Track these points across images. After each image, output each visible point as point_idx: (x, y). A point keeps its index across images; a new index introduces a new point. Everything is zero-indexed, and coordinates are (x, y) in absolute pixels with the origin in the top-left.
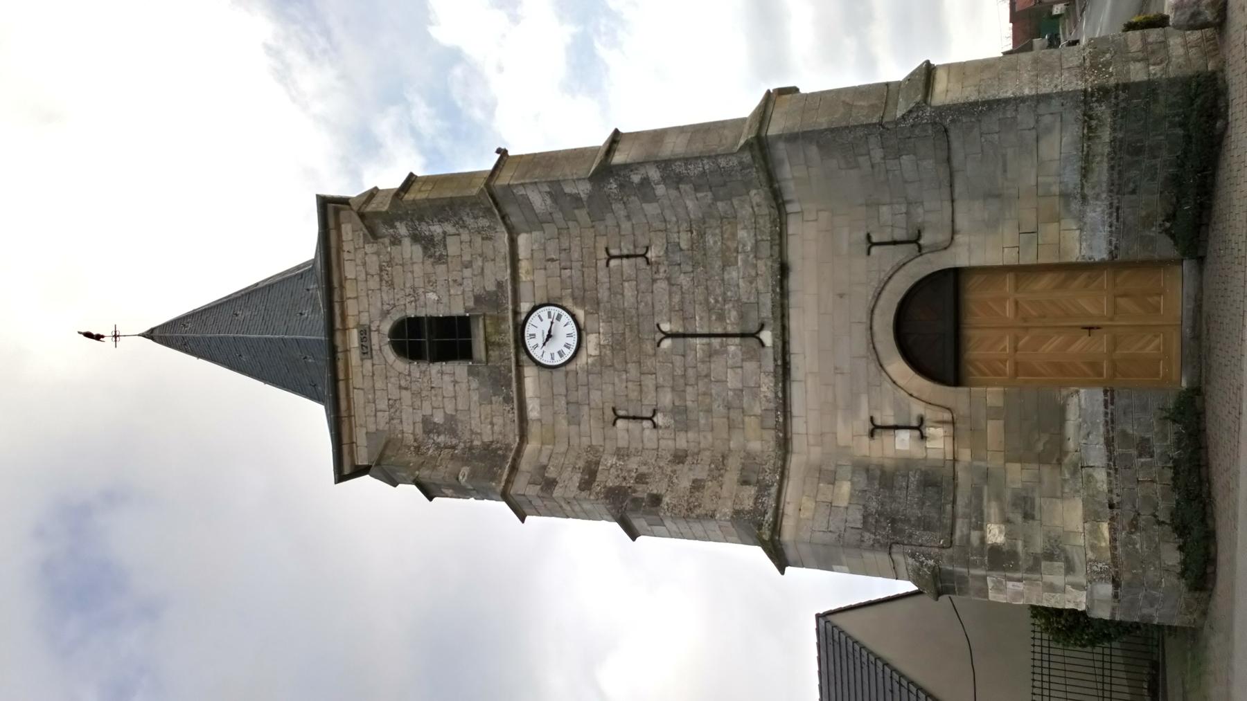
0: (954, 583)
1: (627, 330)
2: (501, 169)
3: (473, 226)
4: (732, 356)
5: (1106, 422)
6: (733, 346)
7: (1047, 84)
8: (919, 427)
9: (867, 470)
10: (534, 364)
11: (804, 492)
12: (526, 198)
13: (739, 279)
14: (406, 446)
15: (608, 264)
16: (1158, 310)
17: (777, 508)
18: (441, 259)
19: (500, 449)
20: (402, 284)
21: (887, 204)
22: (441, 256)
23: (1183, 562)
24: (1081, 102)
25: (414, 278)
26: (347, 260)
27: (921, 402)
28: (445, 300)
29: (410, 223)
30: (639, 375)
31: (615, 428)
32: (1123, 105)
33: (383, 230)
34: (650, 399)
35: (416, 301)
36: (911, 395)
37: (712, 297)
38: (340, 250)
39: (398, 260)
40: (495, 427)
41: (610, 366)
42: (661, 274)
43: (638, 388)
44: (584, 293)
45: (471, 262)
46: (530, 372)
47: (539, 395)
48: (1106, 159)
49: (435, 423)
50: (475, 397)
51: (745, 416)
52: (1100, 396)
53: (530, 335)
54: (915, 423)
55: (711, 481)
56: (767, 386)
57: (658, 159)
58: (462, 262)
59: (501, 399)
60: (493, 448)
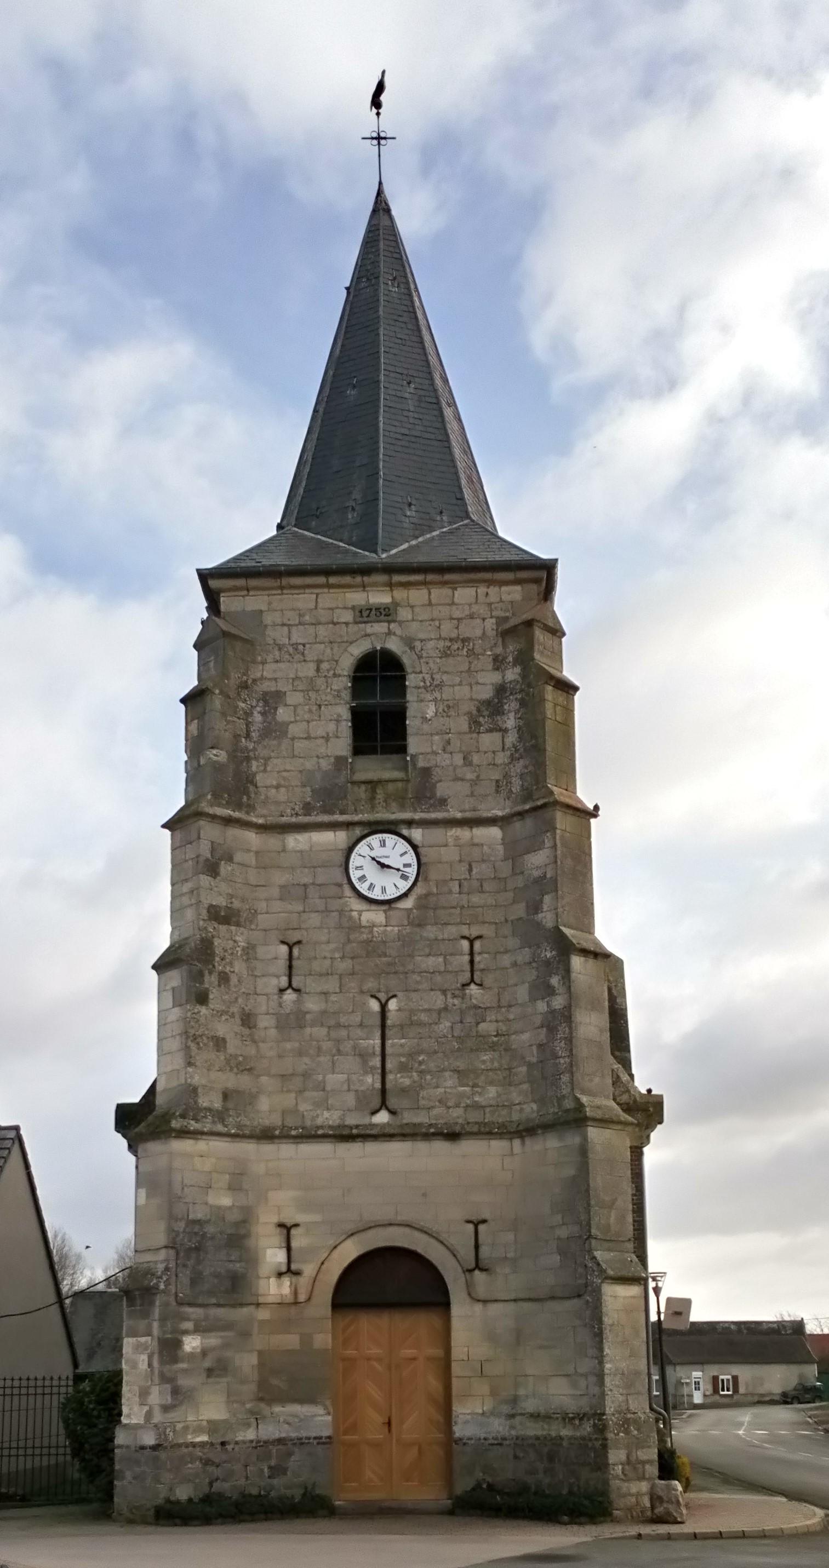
0: (140, 1306)
1: (390, 959)
2: (574, 815)
3: (512, 770)
4: (362, 1080)
5: (301, 1439)
6: (372, 1081)
7: (613, 1383)
8: (290, 1271)
9: (244, 1221)
10: (350, 845)
13: (445, 1088)
14: (247, 670)
15: (464, 937)
16: (407, 1481)
17: (203, 1133)
18: (474, 724)
19: (249, 798)
20: (446, 669)
22: (479, 724)
23: (178, 1502)
24: (595, 1411)
25: (453, 686)
26: (476, 592)
27: (315, 1273)
28: (426, 727)
29: (518, 687)
30: (339, 972)
31: (278, 943)
32: (590, 1444)
33: (513, 647)
34: (312, 985)
35: (425, 688)
36: (323, 1263)
37: (426, 1058)
38: (490, 583)
39: (476, 665)
40: (274, 791)
42: (451, 1000)
43: (324, 971)
44: (432, 908)
46: (340, 838)
47: (314, 849)
48: (545, 1433)
49: (276, 709)
50: (309, 765)
51: (296, 1092)
52: (326, 1433)
53: (384, 841)
54: (293, 1267)
55: (225, 1059)
56: (329, 1118)
57: (573, 1008)
58: (469, 753)
59: (309, 799)
60: (248, 788)
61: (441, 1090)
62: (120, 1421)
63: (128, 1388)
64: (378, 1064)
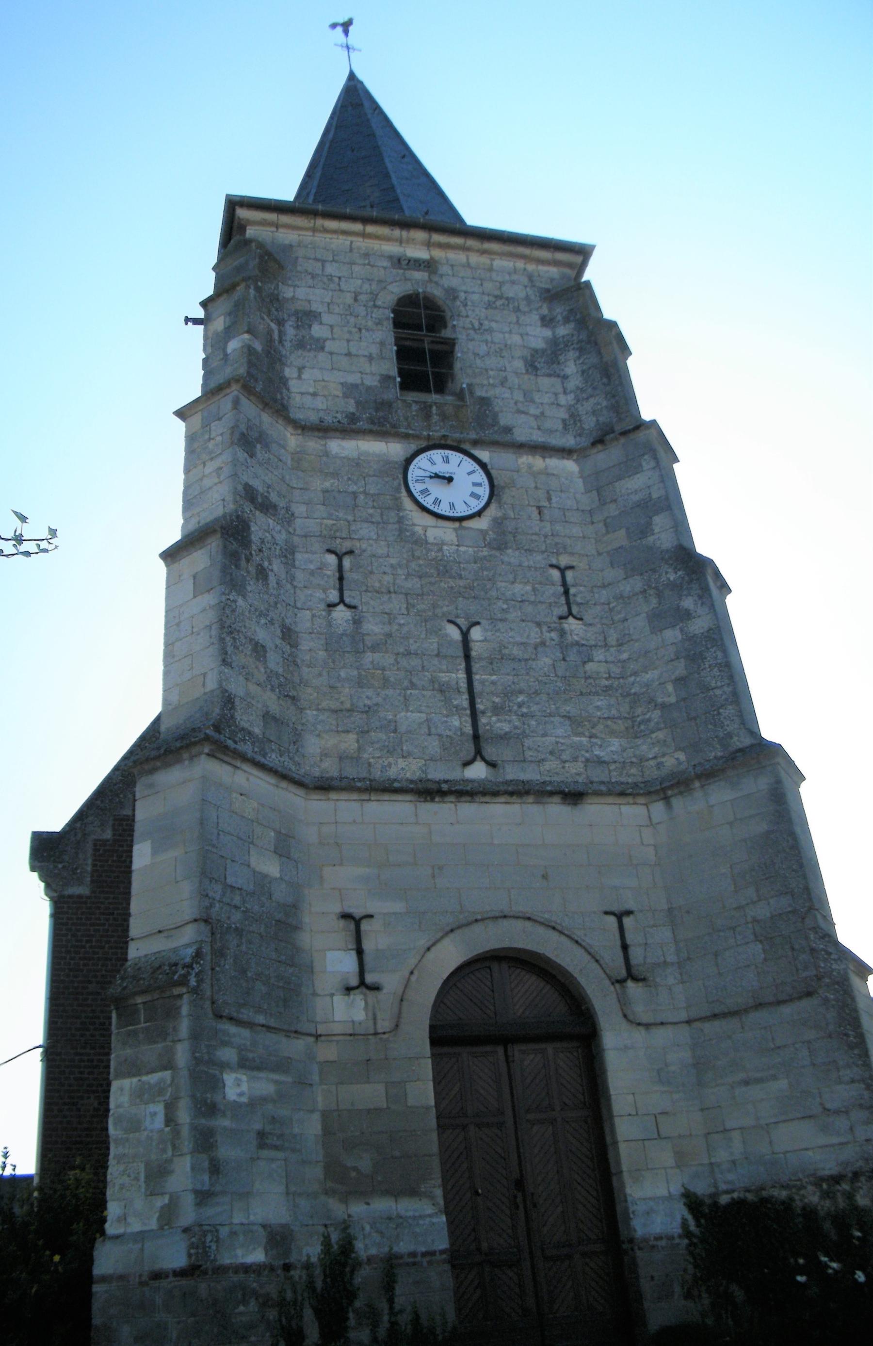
6: (461, 723)
10: (409, 456)
11: (263, 805)
12: (638, 469)
18: (532, 366)
21: (675, 936)
37: (526, 699)
41: (413, 556)
42: (548, 634)
45: (532, 401)
46: (395, 449)
53: (447, 457)
61: (550, 739)
62: (103, 1233)
63: (122, 1168)
64: (466, 704)
